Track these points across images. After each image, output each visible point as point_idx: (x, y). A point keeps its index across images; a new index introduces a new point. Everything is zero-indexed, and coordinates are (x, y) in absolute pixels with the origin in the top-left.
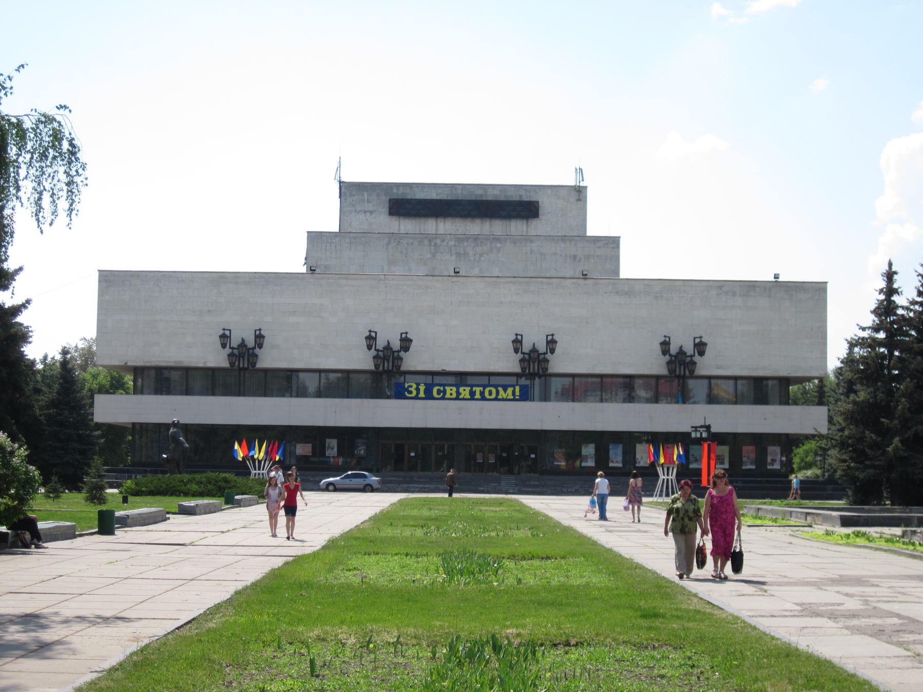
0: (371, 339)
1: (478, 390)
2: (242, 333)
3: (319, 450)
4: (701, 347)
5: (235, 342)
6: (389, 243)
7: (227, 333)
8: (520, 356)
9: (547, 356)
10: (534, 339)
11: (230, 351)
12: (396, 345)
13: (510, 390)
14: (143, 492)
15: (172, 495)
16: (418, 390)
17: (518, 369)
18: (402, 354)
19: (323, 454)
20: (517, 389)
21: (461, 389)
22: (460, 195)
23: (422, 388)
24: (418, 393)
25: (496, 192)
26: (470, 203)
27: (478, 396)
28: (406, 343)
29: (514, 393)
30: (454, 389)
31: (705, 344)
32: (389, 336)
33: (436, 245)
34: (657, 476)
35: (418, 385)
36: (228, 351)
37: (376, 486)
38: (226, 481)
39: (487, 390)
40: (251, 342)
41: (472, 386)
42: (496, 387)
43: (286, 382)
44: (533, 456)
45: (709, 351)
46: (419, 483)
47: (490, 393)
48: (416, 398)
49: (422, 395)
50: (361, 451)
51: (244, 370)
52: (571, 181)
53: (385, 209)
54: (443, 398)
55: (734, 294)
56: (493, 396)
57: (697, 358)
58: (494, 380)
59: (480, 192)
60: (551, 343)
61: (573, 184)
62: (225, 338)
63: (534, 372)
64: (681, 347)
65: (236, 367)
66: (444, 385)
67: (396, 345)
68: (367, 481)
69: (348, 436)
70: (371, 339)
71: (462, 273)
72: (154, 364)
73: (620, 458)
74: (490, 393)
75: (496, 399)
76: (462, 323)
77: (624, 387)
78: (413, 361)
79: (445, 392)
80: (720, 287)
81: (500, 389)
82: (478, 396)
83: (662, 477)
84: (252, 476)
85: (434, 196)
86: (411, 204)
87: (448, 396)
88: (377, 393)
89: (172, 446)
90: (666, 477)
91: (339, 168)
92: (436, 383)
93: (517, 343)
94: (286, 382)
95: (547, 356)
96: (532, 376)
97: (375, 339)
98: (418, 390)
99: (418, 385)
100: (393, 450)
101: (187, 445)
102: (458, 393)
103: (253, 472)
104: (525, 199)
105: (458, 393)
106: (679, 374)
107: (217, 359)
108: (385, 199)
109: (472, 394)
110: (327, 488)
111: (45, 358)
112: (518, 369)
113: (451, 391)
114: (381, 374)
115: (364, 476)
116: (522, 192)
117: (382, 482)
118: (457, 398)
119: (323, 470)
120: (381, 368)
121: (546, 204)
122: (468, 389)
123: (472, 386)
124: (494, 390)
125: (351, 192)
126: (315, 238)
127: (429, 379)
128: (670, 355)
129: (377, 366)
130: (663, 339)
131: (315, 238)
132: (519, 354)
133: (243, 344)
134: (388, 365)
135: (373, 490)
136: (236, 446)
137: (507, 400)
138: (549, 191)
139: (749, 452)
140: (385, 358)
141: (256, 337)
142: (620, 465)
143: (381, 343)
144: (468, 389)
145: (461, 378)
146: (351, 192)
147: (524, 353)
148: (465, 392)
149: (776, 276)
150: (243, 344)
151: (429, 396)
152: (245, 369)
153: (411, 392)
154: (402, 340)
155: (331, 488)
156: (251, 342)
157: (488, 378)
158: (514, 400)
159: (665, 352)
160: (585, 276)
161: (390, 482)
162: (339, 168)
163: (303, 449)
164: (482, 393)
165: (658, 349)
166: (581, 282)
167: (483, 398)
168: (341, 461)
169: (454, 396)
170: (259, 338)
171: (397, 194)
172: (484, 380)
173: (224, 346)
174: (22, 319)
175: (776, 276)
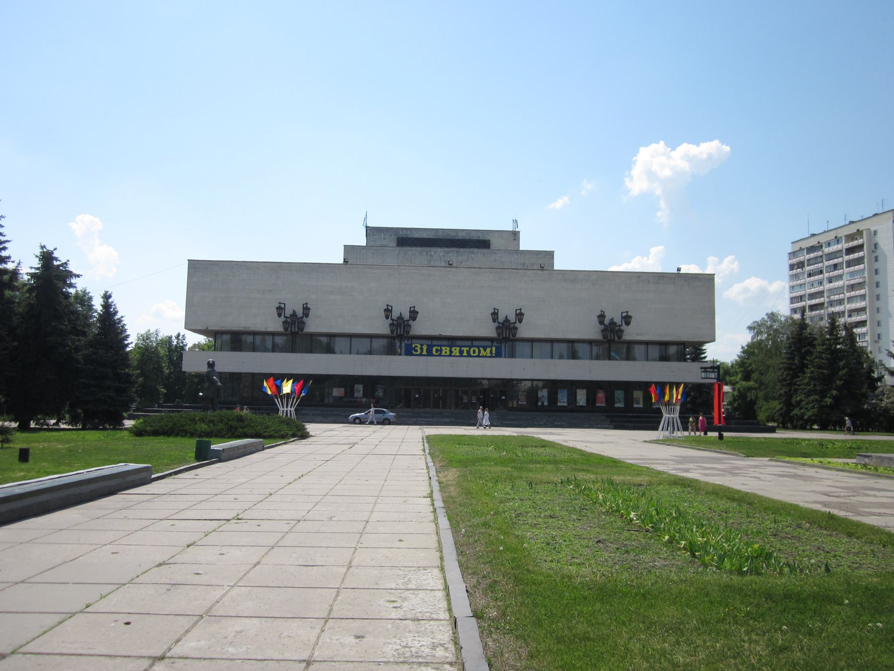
0: (388, 311)
1: (465, 349)
2: (294, 306)
3: (350, 392)
4: (627, 319)
5: (288, 312)
6: (399, 253)
7: (283, 306)
8: (496, 324)
10: (507, 312)
12: (406, 316)
13: (488, 350)
14: (146, 431)
15: (177, 435)
16: (422, 349)
17: (493, 334)
18: (411, 322)
19: (353, 396)
20: (494, 349)
21: (453, 349)
22: (441, 236)
23: (425, 348)
24: (422, 351)
25: (463, 234)
26: (447, 240)
27: (465, 354)
28: (414, 314)
29: (491, 352)
30: (448, 349)
31: (631, 317)
32: (401, 310)
33: (431, 255)
35: (422, 345)
36: (282, 319)
37: (392, 420)
38: (240, 419)
39: (472, 350)
40: (300, 313)
41: (461, 347)
42: (478, 347)
43: (325, 343)
44: (503, 398)
46: (425, 417)
47: (474, 352)
48: (421, 355)
49: (425, 352)
50: (380, 393)
51: (295, 334)
52: (510, 228)
53: (394, 244)
54: (440, 355)
55: (649, 282)
56: (476, 354)
57: (624, 327)
58: (475, 343)
59: (454, 234)
60: (520, 316)
61: (511, 229)
62: (280, 310)
63: (506, 337)
65: (289, 332)
66: (441, 346)
67: (406, 316)
68: (386, 416)
69: (371, 382)
70: (388, 311)
71: (455, 265)
72: (228, 329)
73: (565, 400)
74: (474, 352)
75: (478, 356)
76: (454, 305)
77: (571, 348)
78: (419, 328)
79: (441, 350)
80: (639, 277)
81: (482, 349)
82: (465, 354)
84: (280, 413)
85: (425, 236)
86: (407, 240)
87: (443, 353)
88: (391, 351)
89: (206, 385)
91: (365, 219)
92: (436, 343)
93: (495, 315)
94: (325, 343)
96: (506, 340)
97: (391, 311)
98: (422, 349)
99: (422, 345)
100: (403, 394)
101: (219, 384)
102: (451, 352)
103: (281, 409)
104: (481, 238)
105: (451, 352)
106: (612, 340)
107: (275, 325)
108: (394, 238)
109: (461, 352)
110: (354, 422)
111: (179, 335)
112: (493, 334)
113: (446, 350)
114: (394, 338)
115: (384, 412)
116: (480, 234)
117: (397, 417)
118: (450, 355)
119: (356, 407)
121: (495, 243)
122: (458, 349)
123: (461, 347)
124: (477, 350)
125: (371, 232)
126: (348, 249)
127: (429, 342)
129: (392, 332)
130: (600, 313)
131: (348, 249)
133: (294, 314)
134: (400, 331)
135: (390, 423)
136: (265, 384)
137: (486, 357)
138: (496, 234)
139: (619, 394)
140: (398, 325)
141: (304, 308)
142: (566, 404)
144: (458, 349)
145: (452, 341)
146: (371, 232)
147: (393, 320)
148: (456, 350)
149: (679, 269)
150: (294, 314)
151: (430, 353)
152: (296, 333)
153: (416, 351)
154: (411, 312)
155: (357, 421)
156: (300, 313)
157: (471, 340)
158: (491, 357)
159: (601, 322)
160: (542, 268)
161: (403, 416)
162: (365, 219)
163: (337, 392)
164: (468, 352)
165: (595, 320)
166: (540, 272)
167: (469, 355)
168: (364, 400)
169: (448, 353)
170: (306, 310)
171: (401, 234)
172: (469, 343)
174: (39, 254)
175: (679, 269)
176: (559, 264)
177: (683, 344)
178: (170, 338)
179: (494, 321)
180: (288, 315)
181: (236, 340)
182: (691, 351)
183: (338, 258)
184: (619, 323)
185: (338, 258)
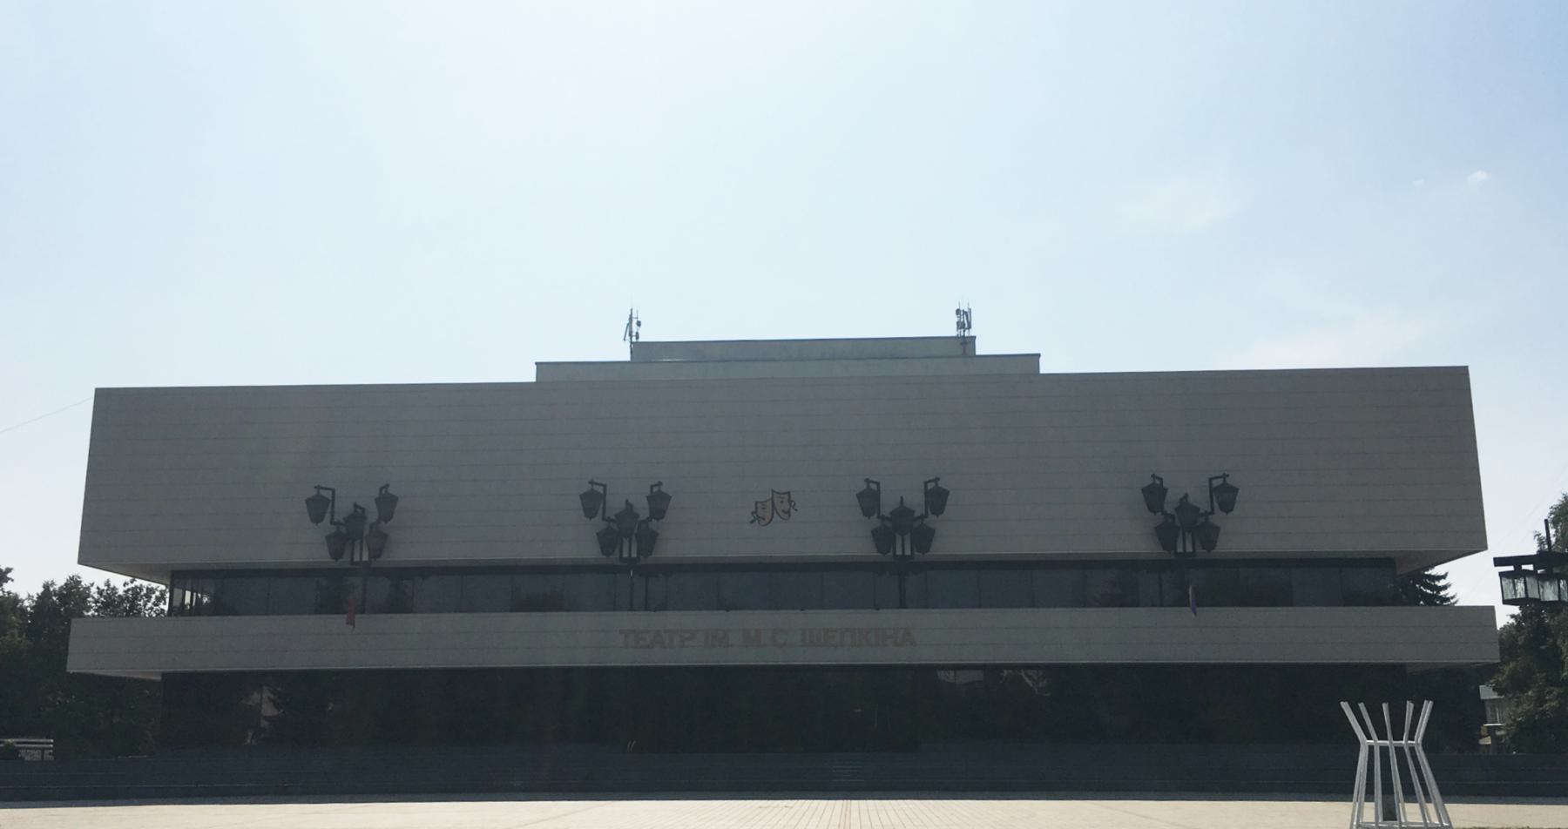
9: (1213, 519)
11: (333, 529)
12: (916, 501)
18: (654, 524)
34: (1356, 743)
43: (405, 589)
45: (950, 510)
57: (1218, 518)
64: (1186, 496)
77: (535, 587)
83: (1365, 743)
90: (1376, 742)
94: (405, 589)
95: (1213, 519)
97: (603, 496)
106: (1186, 554)
107: (1129, 536)
120: (616, 556)
128: (1164, 513)
130: (862, 486)
132: (874, 518)
143: (888, 504)
147: (883, 518)
154: (927, 493)
170: (659, 501)
173: (590, 513)
176: (1046, 367)
177: (1385, 562)
178: (1502, 575)
179: (867, 512)
180: (886, 511)
181: (222, 588)
182: (1405, 582)
183: (530, 376)
184: (1204, 507)
185: (530, 376)
